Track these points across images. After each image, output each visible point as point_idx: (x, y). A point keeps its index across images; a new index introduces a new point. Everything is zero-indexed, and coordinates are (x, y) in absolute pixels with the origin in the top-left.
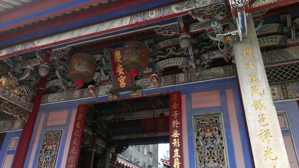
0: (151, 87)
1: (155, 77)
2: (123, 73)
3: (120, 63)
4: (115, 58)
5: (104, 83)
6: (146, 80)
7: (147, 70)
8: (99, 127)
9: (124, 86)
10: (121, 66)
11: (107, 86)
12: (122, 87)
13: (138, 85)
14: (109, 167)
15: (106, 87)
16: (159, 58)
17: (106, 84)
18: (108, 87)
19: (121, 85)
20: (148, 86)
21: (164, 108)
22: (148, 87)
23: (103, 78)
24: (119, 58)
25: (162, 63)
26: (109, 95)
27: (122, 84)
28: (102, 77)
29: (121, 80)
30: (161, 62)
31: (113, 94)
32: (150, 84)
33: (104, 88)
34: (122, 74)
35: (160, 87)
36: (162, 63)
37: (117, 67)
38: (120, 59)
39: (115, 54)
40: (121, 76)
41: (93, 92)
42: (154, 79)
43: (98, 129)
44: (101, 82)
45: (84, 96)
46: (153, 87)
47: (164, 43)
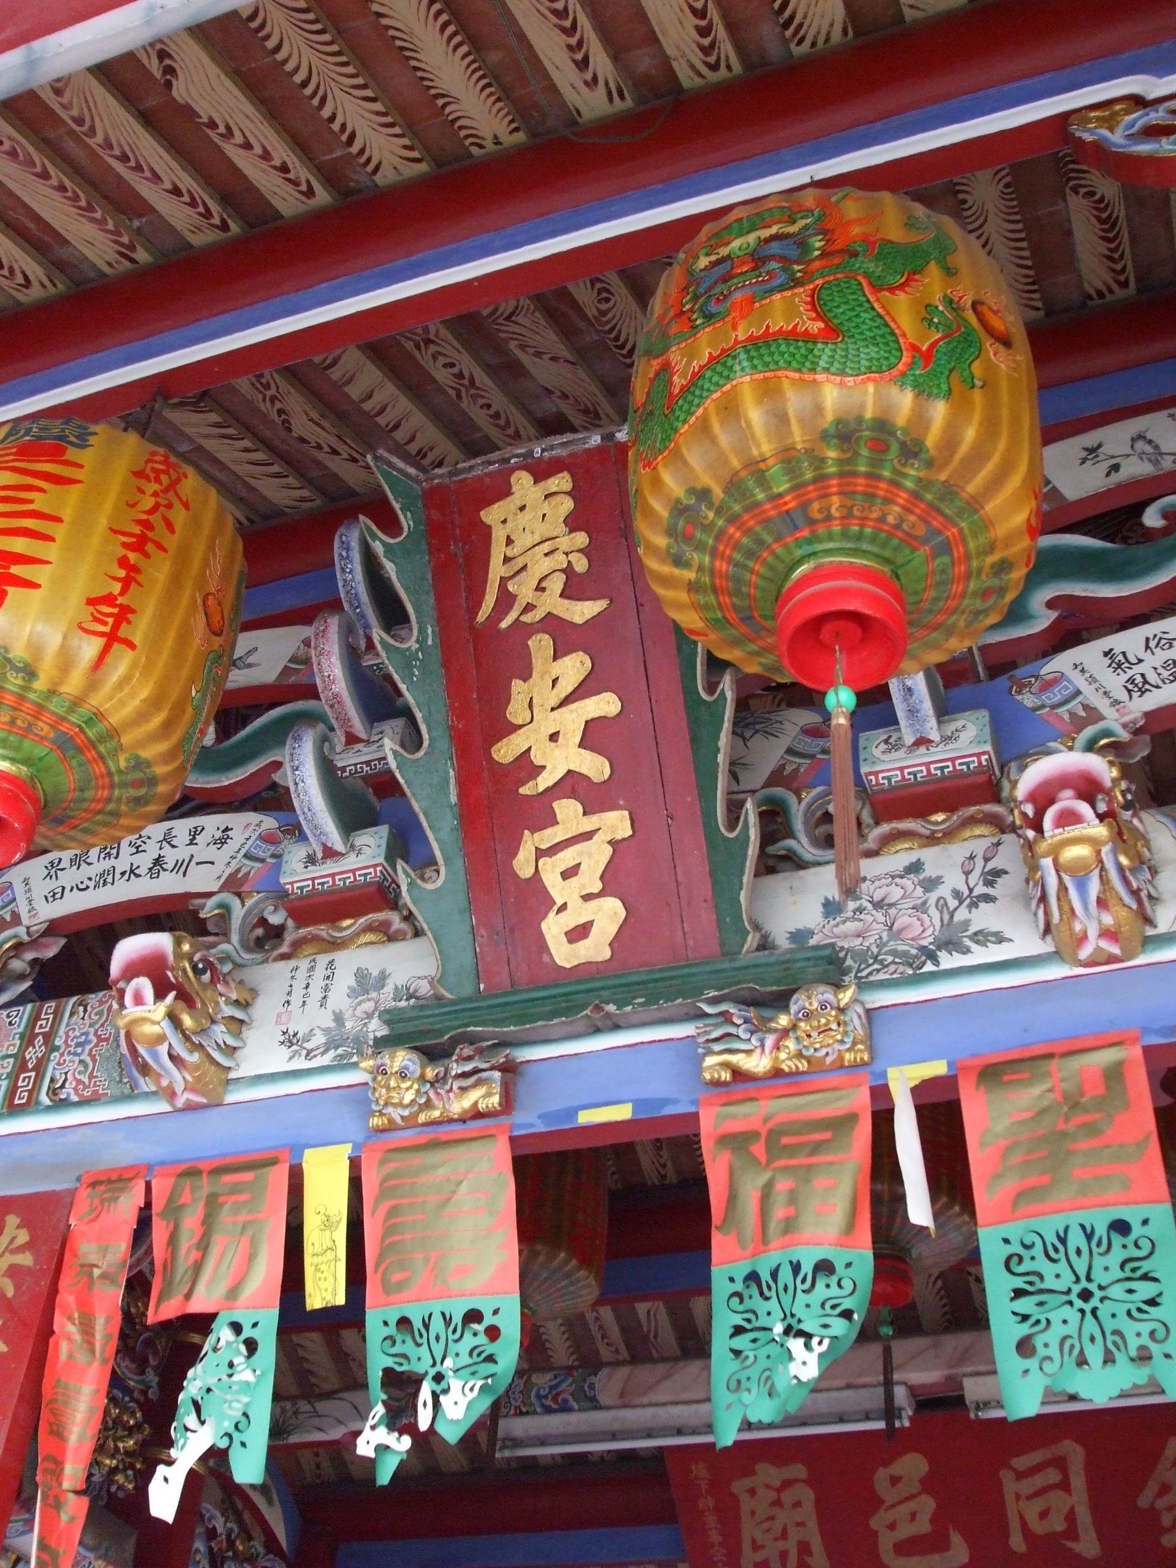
0: (981, 955)
1: (1088, 788)
2: (595, 767)
3: (553, 624)
4: (497, 570)
5: (322, 930)
6: (915, 868)
7: (922, 741)
8: (219, 1524)
9: (596, 948)
10: (574, 668)
11: (348, 962)
12: (564, 955)
13: (799, 937)
14: (135, 1566)
15: (345, 980)
16: (1050, 604)
17: (336, 945)
18: (361, 976)
19: (553, 928)
20: (951, 944)
21: (935, 1332)
22: (948, 961)
23: (311, 860)
24: (545, 565)
25: (1118, 662)
26: (381, 1071)
27: (570, 920)
28: (295, 856)
29: (567, 858)
30: (1090, 654)
31: (432, 1054)
32: (983, 918)
33: (318, 982)
34: (572, 784)
35: (1148, 942)
36: (1118, 662)
37: (517, 685)
38: (557, 584)
39: (491, 515)
40: (568, 811)
41: (173, 1017)
42: (1068, 818)
43: (199, 1545)
44: (275, 919)
45: (53, 1092)
46: (1037, 946)
47: (1092, 450)
